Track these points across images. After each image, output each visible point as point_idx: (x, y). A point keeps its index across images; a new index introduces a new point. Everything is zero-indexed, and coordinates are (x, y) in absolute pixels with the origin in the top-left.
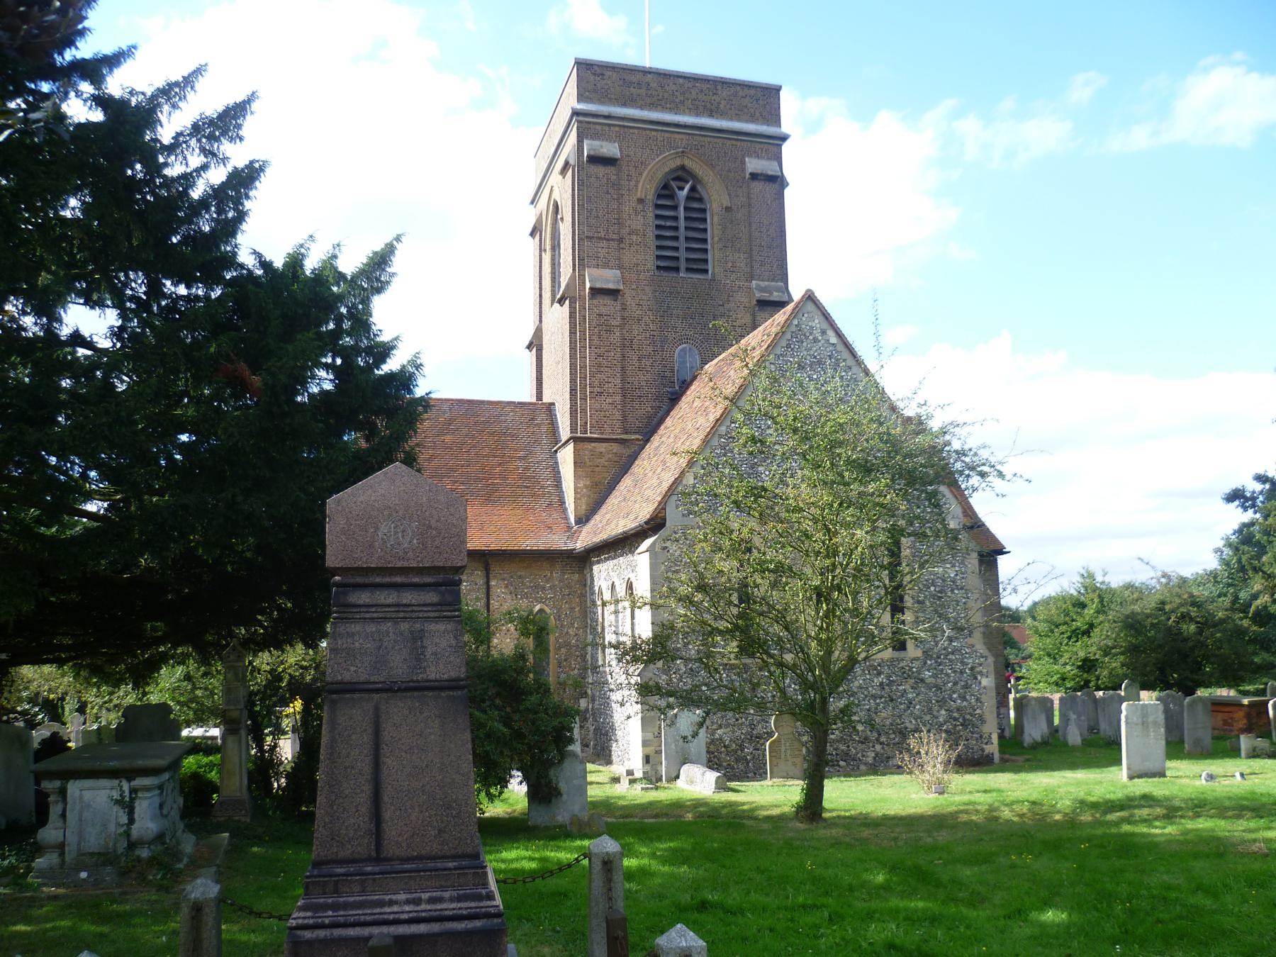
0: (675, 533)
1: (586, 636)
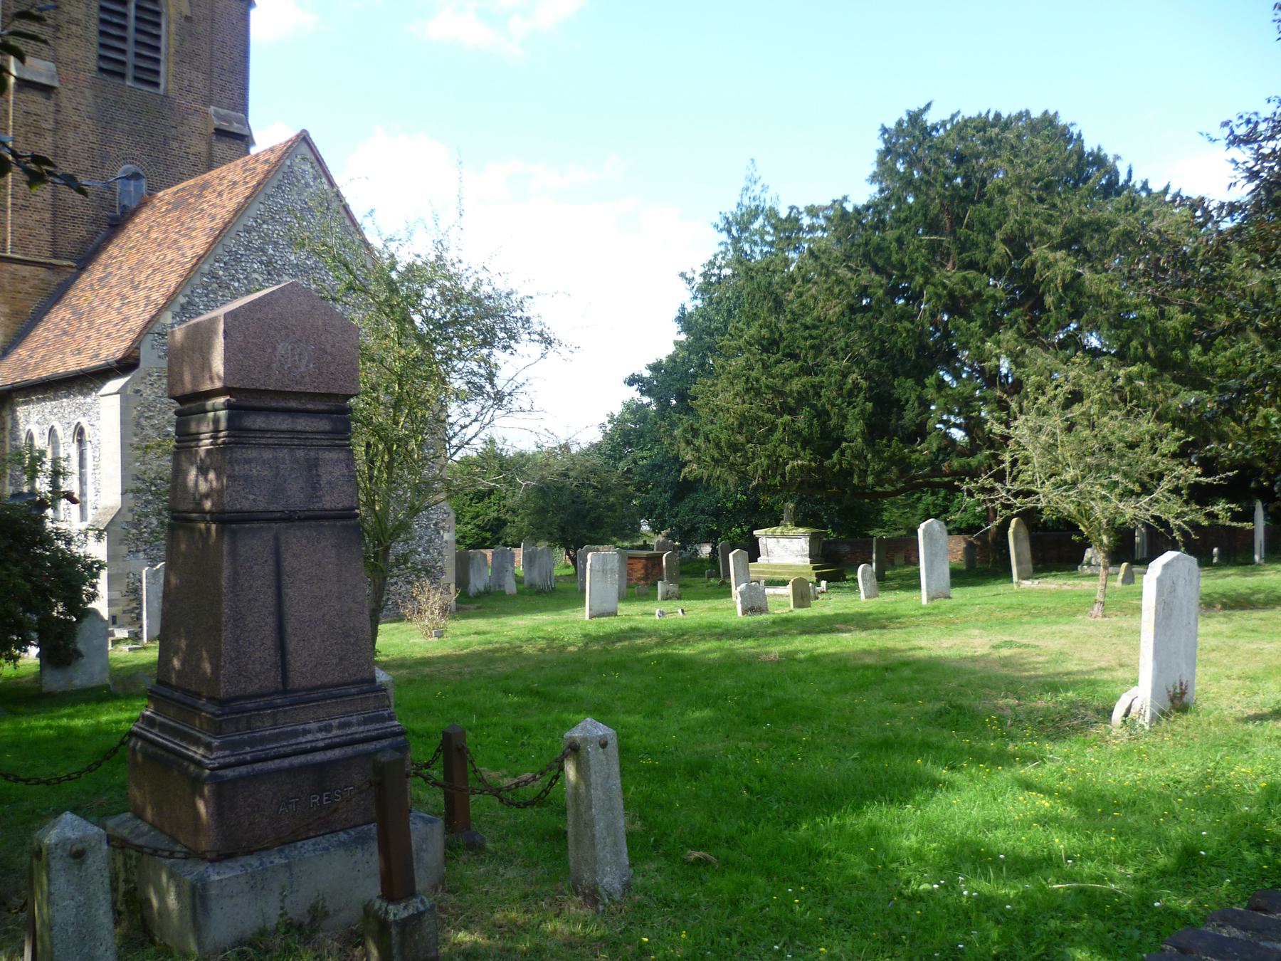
0: (150, 375)
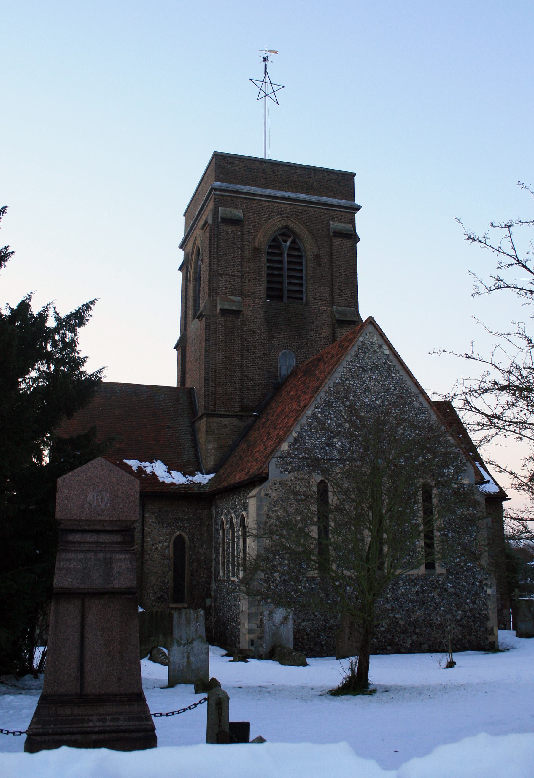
1: (212, 554)
